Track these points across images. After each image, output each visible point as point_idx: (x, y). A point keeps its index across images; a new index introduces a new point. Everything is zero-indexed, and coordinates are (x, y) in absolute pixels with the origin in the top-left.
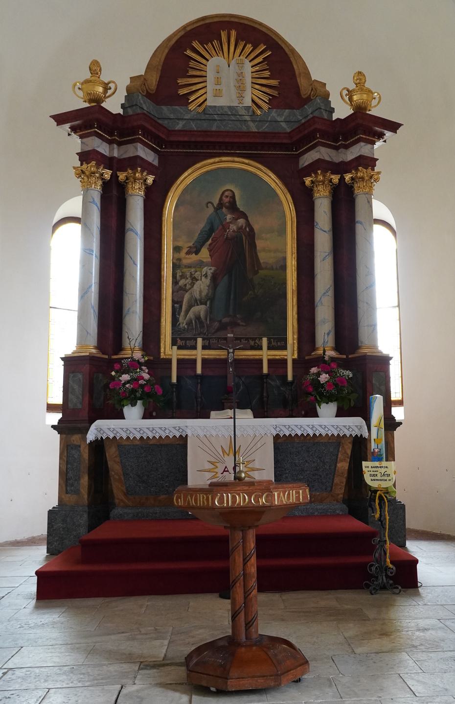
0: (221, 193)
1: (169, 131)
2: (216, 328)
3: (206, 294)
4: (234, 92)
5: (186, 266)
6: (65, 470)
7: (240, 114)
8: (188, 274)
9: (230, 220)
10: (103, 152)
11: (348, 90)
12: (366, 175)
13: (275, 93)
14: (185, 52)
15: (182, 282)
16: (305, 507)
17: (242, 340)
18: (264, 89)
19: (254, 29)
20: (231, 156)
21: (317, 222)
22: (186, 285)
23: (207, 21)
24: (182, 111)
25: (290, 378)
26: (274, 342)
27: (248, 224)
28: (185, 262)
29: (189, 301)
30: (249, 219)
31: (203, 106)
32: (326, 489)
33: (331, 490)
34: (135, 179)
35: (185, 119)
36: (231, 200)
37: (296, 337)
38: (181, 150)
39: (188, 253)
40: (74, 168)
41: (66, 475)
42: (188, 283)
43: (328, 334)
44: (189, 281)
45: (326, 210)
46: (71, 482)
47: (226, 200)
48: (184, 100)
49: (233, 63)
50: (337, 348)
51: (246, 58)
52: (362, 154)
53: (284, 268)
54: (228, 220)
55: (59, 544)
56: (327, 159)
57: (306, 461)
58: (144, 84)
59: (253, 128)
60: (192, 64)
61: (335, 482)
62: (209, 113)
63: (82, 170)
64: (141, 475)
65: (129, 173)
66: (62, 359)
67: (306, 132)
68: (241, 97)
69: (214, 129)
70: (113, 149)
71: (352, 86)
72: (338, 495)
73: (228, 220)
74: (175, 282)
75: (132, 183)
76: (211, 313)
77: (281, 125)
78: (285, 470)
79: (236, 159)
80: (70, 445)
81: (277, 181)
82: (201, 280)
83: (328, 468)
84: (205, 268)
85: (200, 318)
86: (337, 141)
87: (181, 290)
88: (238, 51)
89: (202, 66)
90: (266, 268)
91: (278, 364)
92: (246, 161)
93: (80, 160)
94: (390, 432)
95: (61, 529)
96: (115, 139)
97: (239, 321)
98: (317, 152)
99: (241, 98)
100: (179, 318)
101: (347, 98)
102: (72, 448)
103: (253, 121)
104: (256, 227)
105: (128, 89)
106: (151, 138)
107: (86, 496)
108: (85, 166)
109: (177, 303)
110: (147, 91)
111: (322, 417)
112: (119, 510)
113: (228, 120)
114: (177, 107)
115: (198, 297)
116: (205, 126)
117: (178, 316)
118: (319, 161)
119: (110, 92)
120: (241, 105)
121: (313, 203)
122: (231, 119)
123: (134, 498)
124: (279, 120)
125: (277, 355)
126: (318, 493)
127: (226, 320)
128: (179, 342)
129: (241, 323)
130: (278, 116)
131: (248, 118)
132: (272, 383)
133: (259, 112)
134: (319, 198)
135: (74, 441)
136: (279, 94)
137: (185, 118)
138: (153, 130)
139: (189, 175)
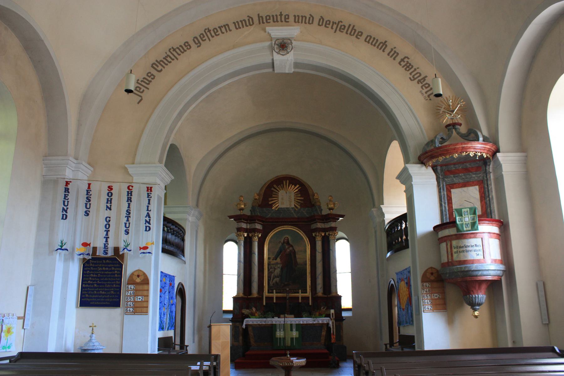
8: (273, 267)
10: (245, 227)
15: (271, 270)
18: (298, 201)
19: (295, 179)
25: (310, 304)
26: (77, 251)
27: (293, 249)
28: (272, 263)
30: (294, 247)
34: (255, 236)
37: (310, 289)
39: (273, 260)
44: (273, 269)
47: (286, 241)
48: (271, 206)
50: (324, 293)
53: (306, 264)
56: (321, 227)
59: (295, 216)
60: (274, 193)
62: (280, 210)
66: (233, 298)
68: (290, 205)
70: (247, 225)
73: (286, 248)
74: (269, 270)
91: (305, 299)
104: (296, 250)
108: (239, 232)
109: (269, 277)
115: (276, 275)
127: (286, 283)
128: (270, 291)
131: (293, 212)
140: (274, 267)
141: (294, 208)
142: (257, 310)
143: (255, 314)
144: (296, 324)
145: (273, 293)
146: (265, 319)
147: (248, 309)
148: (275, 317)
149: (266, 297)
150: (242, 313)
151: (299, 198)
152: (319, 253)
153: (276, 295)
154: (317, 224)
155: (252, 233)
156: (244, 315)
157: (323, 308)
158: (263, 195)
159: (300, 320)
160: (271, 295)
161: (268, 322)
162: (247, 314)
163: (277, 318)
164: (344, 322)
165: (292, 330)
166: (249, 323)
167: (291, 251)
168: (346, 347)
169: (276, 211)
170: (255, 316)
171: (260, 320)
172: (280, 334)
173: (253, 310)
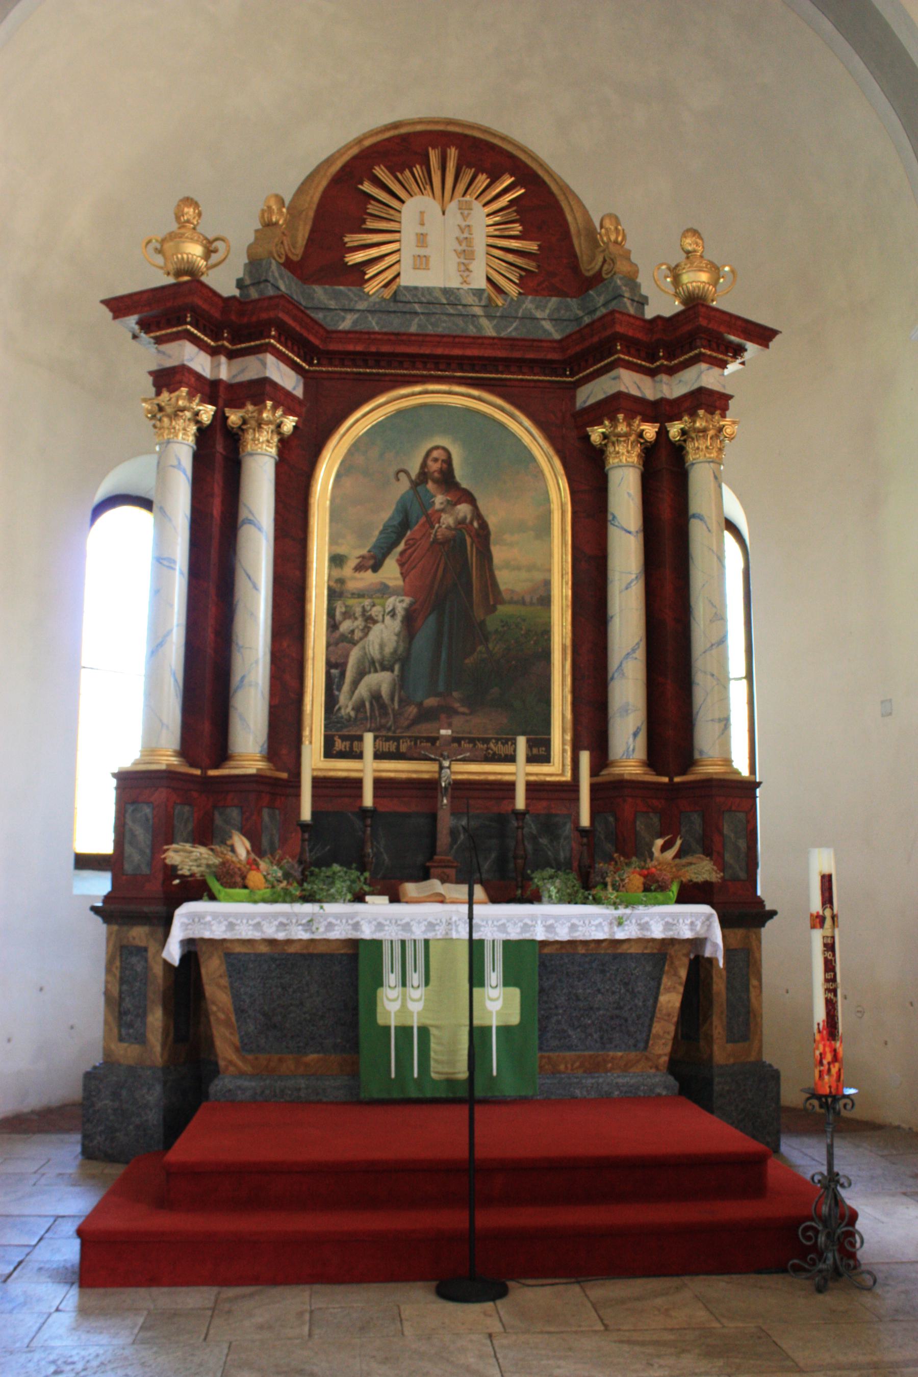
1: (328, 332)
2: (411, 717)
4: (453, 262)
5: (353, 594)
8: (358, 611)
9: (442, 506)
15: (346, 626)
16: (594, 1081)
18: (510, 257)
22: (352, 632)
23: (403, 131)
24: (351, 295)
28: (352, 586)
29: (361, 662)
30: (480, 504)
31: (394, 287)
32: (635, 1046)
33: (646, 1048)
34: (260, 425)
35: (359, 311)
36: (445, 466)
37: (568, 737)
38: (349, 370)
39: (359, 568)
42: (357, 627)
44: (360, 623)
46: (128, 1018)
47: (434, 467)
50: (653, 760)
51: (476, 199)
53: (546, 601)
54: (438, 506)
55: (106, 1140)
56: (635, 392)
59: (489, 329)
60: (372, 208)
61: (654, 1031)
63: (158, 405)
65: (248, 411)
69: (413, 329)
70: (219, 365)
72: (659, 1056)
73: (438, 506)
74: (333, 626)
77: (542, 326)
82: (383, 621)
83: (640, 1004)
86: (653, 358)
87: (342, 641)
88: (461, 186)
89: (392, 212)
90: (511, 602)
92: (475, 393)
96: (223, 346)
97: (457, 705)
100: (338, 697)
104: (492, 521)
107: (158, 1049)
112: (226, 1080)
114: (342, 288)
120: (465, 287)
122: (448, 312)
126: (620, 1054)
127: (431, 702)
128: (339, 745)
129: (462, 709)
131: (478, 311)
135: (134, 938)
140: (364, 610)
141: (483, 291)
142: (257, 849)
143: (244, 878)
144: (507, 944)
146: (308, 908)
147: (204, 844)
148: (368, 898)
149: (317, 782)
150: (166, 865)
151: (514, 244)
152: (630, 532)
153: (375, 771)
154: (617, 378)
156: (177, 882)
157: (664, 848)
158: (311, 214)
159: (533, 918)
160: (342, 768)
161: (330, 926)
162: (195, 869)
163: (385, 899)
164: (769, 930)
165: (476, 978)
166: (207, 935)
167: (461, 522)
168: (775, 1076)
169: (383, 299)
170: (245, 887)
171: (275, 916)
172: (404, 1005)
173: (233, 850)
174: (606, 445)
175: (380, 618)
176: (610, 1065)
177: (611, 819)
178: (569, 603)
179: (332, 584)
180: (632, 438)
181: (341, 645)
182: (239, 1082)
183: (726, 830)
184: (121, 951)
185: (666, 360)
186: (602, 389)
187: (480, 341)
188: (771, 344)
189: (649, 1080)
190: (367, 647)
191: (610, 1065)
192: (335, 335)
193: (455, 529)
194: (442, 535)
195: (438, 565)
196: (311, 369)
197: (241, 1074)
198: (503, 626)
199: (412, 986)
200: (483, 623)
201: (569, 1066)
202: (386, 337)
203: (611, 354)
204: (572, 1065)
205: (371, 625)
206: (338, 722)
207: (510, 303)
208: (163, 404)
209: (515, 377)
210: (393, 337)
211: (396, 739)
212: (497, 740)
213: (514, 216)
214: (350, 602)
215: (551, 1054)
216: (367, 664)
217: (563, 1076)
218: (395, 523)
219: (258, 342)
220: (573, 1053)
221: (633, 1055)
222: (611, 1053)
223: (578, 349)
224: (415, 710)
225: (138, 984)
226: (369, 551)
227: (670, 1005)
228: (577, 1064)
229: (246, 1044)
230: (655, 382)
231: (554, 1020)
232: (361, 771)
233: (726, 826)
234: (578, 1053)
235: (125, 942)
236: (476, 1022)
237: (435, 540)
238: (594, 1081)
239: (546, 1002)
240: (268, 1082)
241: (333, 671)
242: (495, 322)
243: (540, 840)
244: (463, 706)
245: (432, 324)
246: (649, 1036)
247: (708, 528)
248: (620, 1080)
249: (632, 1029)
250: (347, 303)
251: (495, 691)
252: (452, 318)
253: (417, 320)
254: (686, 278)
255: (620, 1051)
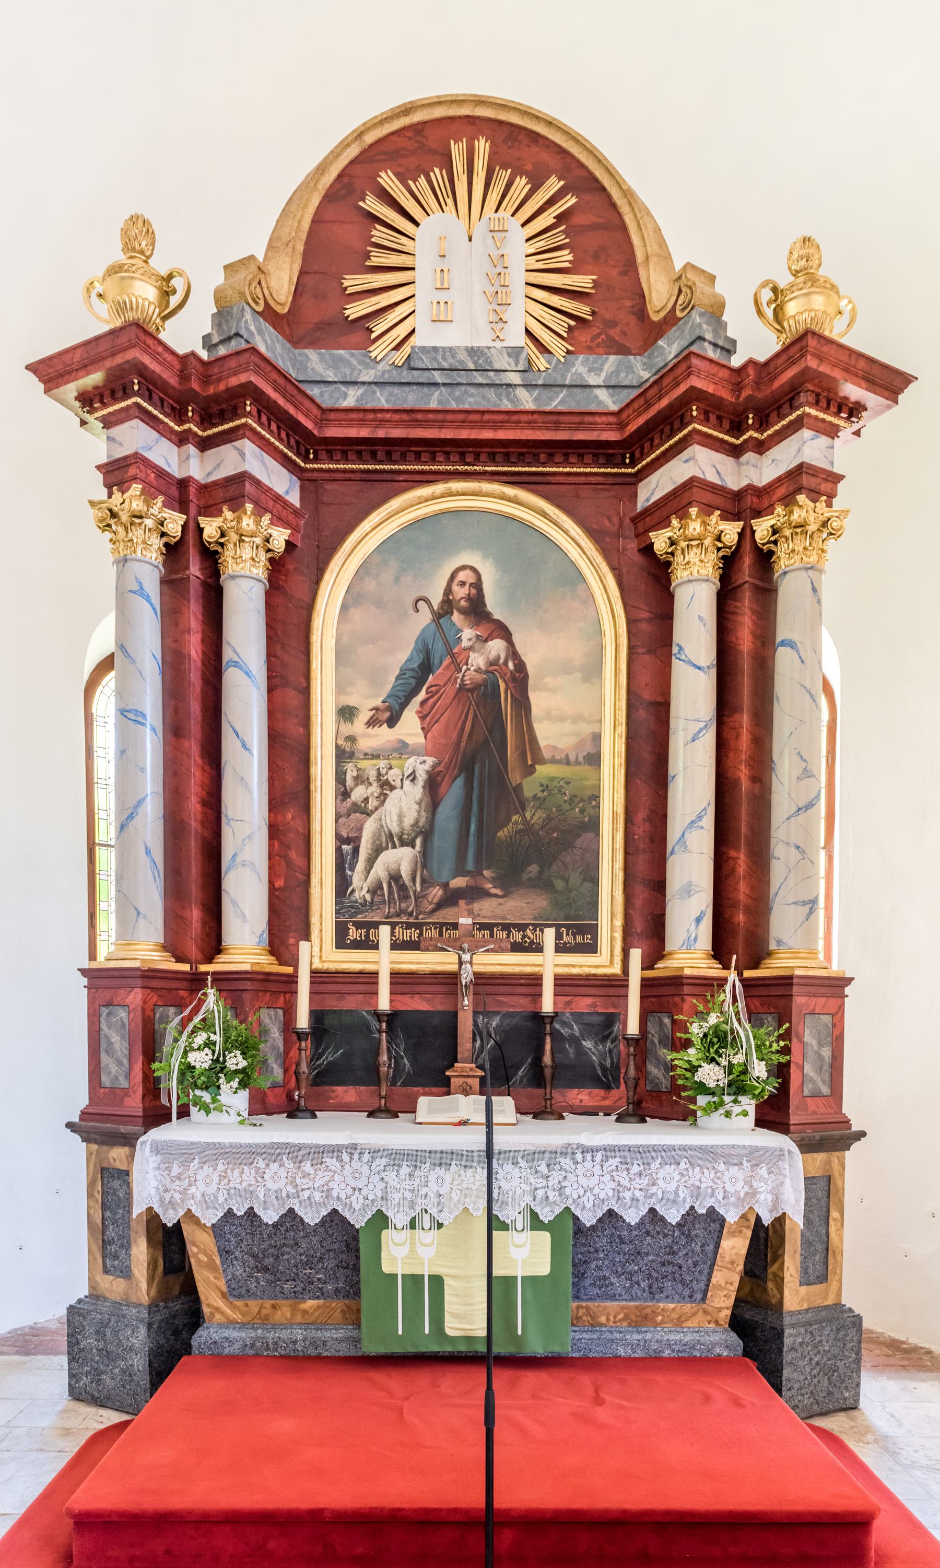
0: (448, 575)
1: (323, 411)
2: (435, 900)
3: (412, 822)
4: (481, 311)
5: (366, 754)
6: (99, 1221)
7: (497, 367)
8: (372, 774)
9: (470, 643)
11: (775, 290)
12: (812, 519)
13: (582, 309)
14: (361, 204)
15: (358, 794)
16: (640, 1337)
17: (495, 929)
18: (556, 301)
20: (473, 480)
21: (678, 645)
22: (366, 800)
23: (417, 117)
24: (354, 362)
26: (567, 934)
27: (513, 653)
28: (365, 744)
29: (376, 837)
30: (516, 639)
31: (406, 349)
32: (691, 1297)
33: (704, 1299)
35: (364, 383)
36: (473, 591)
38: (354, 466)
39: (372, 723)
40: (92, 503)
41: (103, 1234)
42: (372, 794)
43: (698, 920)
44: (375, 789)
45: (703, 615)
46: (113, 1248)
47: (460, 592)
49: (479, 229)
51: (513, 215)
52: (807, 460)
53: (594, 759)
54: (465, 643)
55: (92, 1382)
56: (712, 478)
57: (648, 1233)
58: (259, 283)
59: (527, 401)
60: (379, 234)
61: (714, 1280)
63: (110, 510)
64: (261, 1255)
65: (225, 519)
67: (664, 402)
69: (433, 405)
71: (784, 280)
72: (720, 1309)
73: (465, 643)
74: (343, 793)
75: (235, 544)
76: (424, 866)
77: (596, 397)
78: (596, 1251)
79: (486, 486)
80: (107, 1169)
81: (583, 543)
82: (402, 787)
83: (698, 1248)
84: (412, 759)
85: (401, 877)
86: (737, 428)
87: (355, 812)
88: (494, 197)
89: (404, 240)
90: (553, 761)
92: (510, 491)
93: (105, 485)
94: (837, 1153)
95: (94, 1350)
96: (190, 430)
97: (488, 886)
98: (686, 461)
99: (501, 325)
100: (351, 877)
101: (769, 312)
102: (113, 1176)
103: (528, 386)
104: (531, 661)
105: (219, 297)
106: (269, 420)
107: (144, 1285)
108: (117, 497)
109: (348, 841)
110: (266, 303)
111: (202, 457)
112: (212, 1330)
113: (468, 384)
114: (342, 352)
115: (395, 829)
116: (411, 399)
117: (350, 873)
118: (691, 484)
119: (174, 301)
120: (498, 344)
121: (671, 597)
122: (475, 381)
123: (247, 1305)
124: (592, 383)
125: (574, 966)
126: (672, 1306)
127: (459, 882)
128: (354, 933)
129: (494, 891)
130: (589, 371)
131: (515, 378)
132: (565, 1031)
133: (541, 362)
134: (690, 581)
135: (114, 1160)
136: (593, 313)
137: (361, 379)
138: (281, 401)
139: (373, 529)
140: (379, 774)
145: (370, 945)
149: (314, 973)
155: (219, 513)
167: (494, 663)
174: (672, 554)
175: (398, 783)
176: (660, 1318)
177: (667, 1021)
178: (623, 762)
179: (341, 742)
180: (708, 542)
181: (353, 816)
182: (227, 1333)
183: (807, 1039)
184: (102, 1173)
185: (756, 430)
186: (671, 479)
187: (515, 418)
188: (900, 397)
189: (707, 1337)
190: (383, 817)
191: (660, 1318)
192: (332, 416)
193: (487, 672)
194: (470, 679)
195: (467, 715)
196: (308, 466)
197: (231, 1323)
198: (543, 791)
199: (423, 1229)
200: (518, 789)
201: (612, 1318)
202: (396, 417)
203: (683, 425)
204: (615, 1317)
205: (388, 792)
206: (352, 907)
207: (556, 367)
208: (115, 509)
209: (561, 469)
210: (405, 417)
211: (419, 926)
212: (535, 926)
213: (562, 239)
214: (363, 764)
215: (590, 1304)
216: (384, 839)
217: (604, 1329)
218: (415, 666)
219: (232, 425)
220: (616, 1303)
221: (688, 1307)
222: (662, 1305)
223: (641, 421)
224: (440, 892)
225: (121, 1211)
226: (384, 702)
227: (734, 1251)
228: (621, 1316)
229: (234, 1289)
230: (739, 464)
231: (593, 1266)
232: (377, 963)
233: (807, 1032)
234: (624, 1303)
235: (105, 1165)
236: (496, 1272)
237: (462, 685)
238: (640, 1337)
239: (584, 1245)
240: (260, 1331)
241: (344, 847)
242: (536, 393)
243: (584, 1043)
244: (495, 887)
245: (457, 400)
246: (708, 1286)
247: (800, 657)
248: (672, 1337)
249: (688, 1278)
250: (348, 372)
251: (534, 869)
252: (481, 390)
253: (437, 394)
254: (792, 308)
255: (672, 1302)
